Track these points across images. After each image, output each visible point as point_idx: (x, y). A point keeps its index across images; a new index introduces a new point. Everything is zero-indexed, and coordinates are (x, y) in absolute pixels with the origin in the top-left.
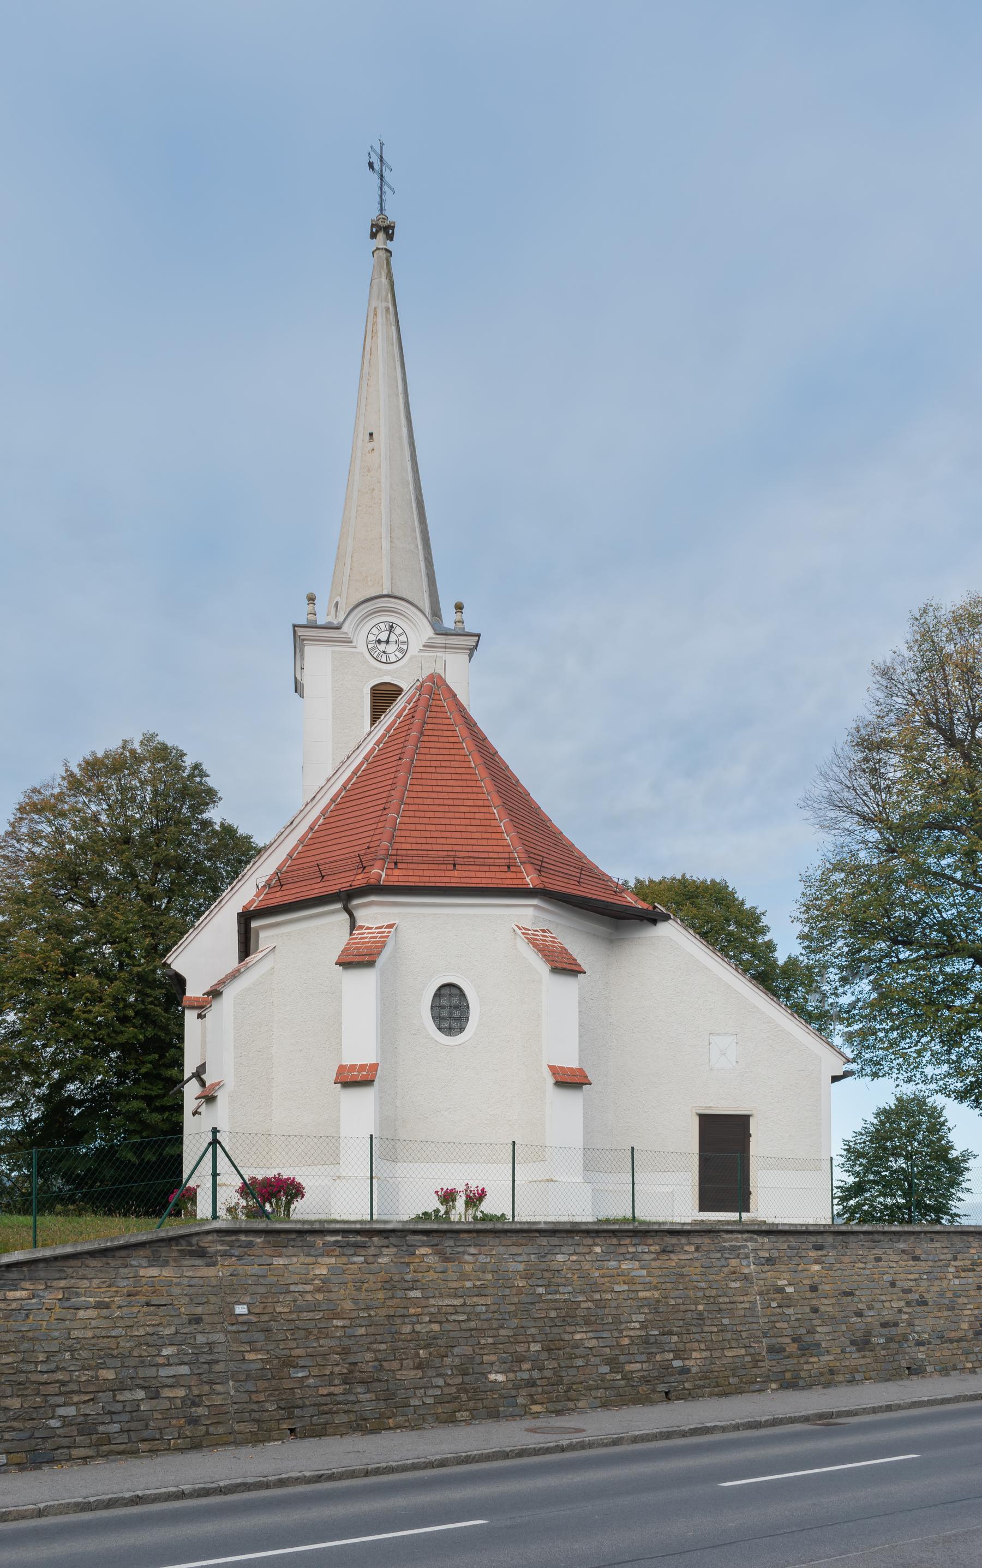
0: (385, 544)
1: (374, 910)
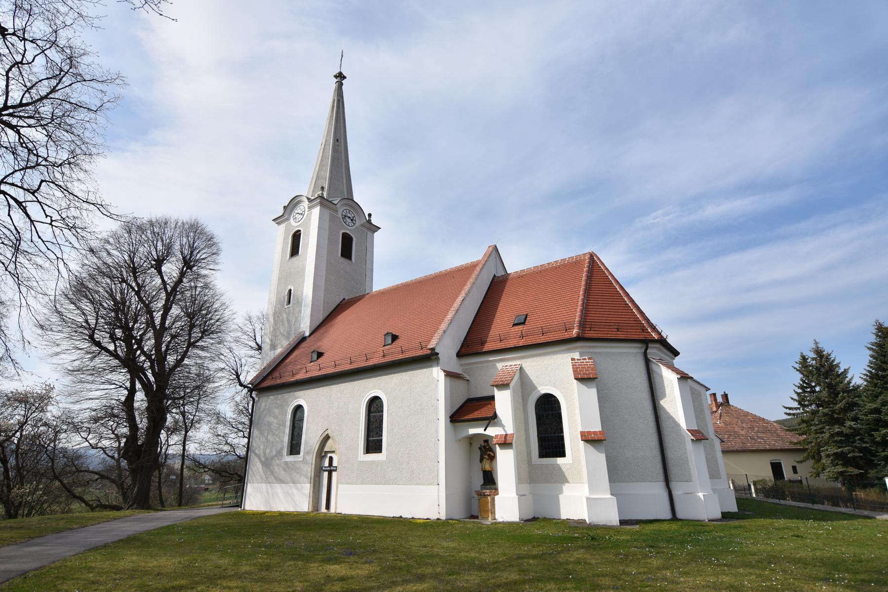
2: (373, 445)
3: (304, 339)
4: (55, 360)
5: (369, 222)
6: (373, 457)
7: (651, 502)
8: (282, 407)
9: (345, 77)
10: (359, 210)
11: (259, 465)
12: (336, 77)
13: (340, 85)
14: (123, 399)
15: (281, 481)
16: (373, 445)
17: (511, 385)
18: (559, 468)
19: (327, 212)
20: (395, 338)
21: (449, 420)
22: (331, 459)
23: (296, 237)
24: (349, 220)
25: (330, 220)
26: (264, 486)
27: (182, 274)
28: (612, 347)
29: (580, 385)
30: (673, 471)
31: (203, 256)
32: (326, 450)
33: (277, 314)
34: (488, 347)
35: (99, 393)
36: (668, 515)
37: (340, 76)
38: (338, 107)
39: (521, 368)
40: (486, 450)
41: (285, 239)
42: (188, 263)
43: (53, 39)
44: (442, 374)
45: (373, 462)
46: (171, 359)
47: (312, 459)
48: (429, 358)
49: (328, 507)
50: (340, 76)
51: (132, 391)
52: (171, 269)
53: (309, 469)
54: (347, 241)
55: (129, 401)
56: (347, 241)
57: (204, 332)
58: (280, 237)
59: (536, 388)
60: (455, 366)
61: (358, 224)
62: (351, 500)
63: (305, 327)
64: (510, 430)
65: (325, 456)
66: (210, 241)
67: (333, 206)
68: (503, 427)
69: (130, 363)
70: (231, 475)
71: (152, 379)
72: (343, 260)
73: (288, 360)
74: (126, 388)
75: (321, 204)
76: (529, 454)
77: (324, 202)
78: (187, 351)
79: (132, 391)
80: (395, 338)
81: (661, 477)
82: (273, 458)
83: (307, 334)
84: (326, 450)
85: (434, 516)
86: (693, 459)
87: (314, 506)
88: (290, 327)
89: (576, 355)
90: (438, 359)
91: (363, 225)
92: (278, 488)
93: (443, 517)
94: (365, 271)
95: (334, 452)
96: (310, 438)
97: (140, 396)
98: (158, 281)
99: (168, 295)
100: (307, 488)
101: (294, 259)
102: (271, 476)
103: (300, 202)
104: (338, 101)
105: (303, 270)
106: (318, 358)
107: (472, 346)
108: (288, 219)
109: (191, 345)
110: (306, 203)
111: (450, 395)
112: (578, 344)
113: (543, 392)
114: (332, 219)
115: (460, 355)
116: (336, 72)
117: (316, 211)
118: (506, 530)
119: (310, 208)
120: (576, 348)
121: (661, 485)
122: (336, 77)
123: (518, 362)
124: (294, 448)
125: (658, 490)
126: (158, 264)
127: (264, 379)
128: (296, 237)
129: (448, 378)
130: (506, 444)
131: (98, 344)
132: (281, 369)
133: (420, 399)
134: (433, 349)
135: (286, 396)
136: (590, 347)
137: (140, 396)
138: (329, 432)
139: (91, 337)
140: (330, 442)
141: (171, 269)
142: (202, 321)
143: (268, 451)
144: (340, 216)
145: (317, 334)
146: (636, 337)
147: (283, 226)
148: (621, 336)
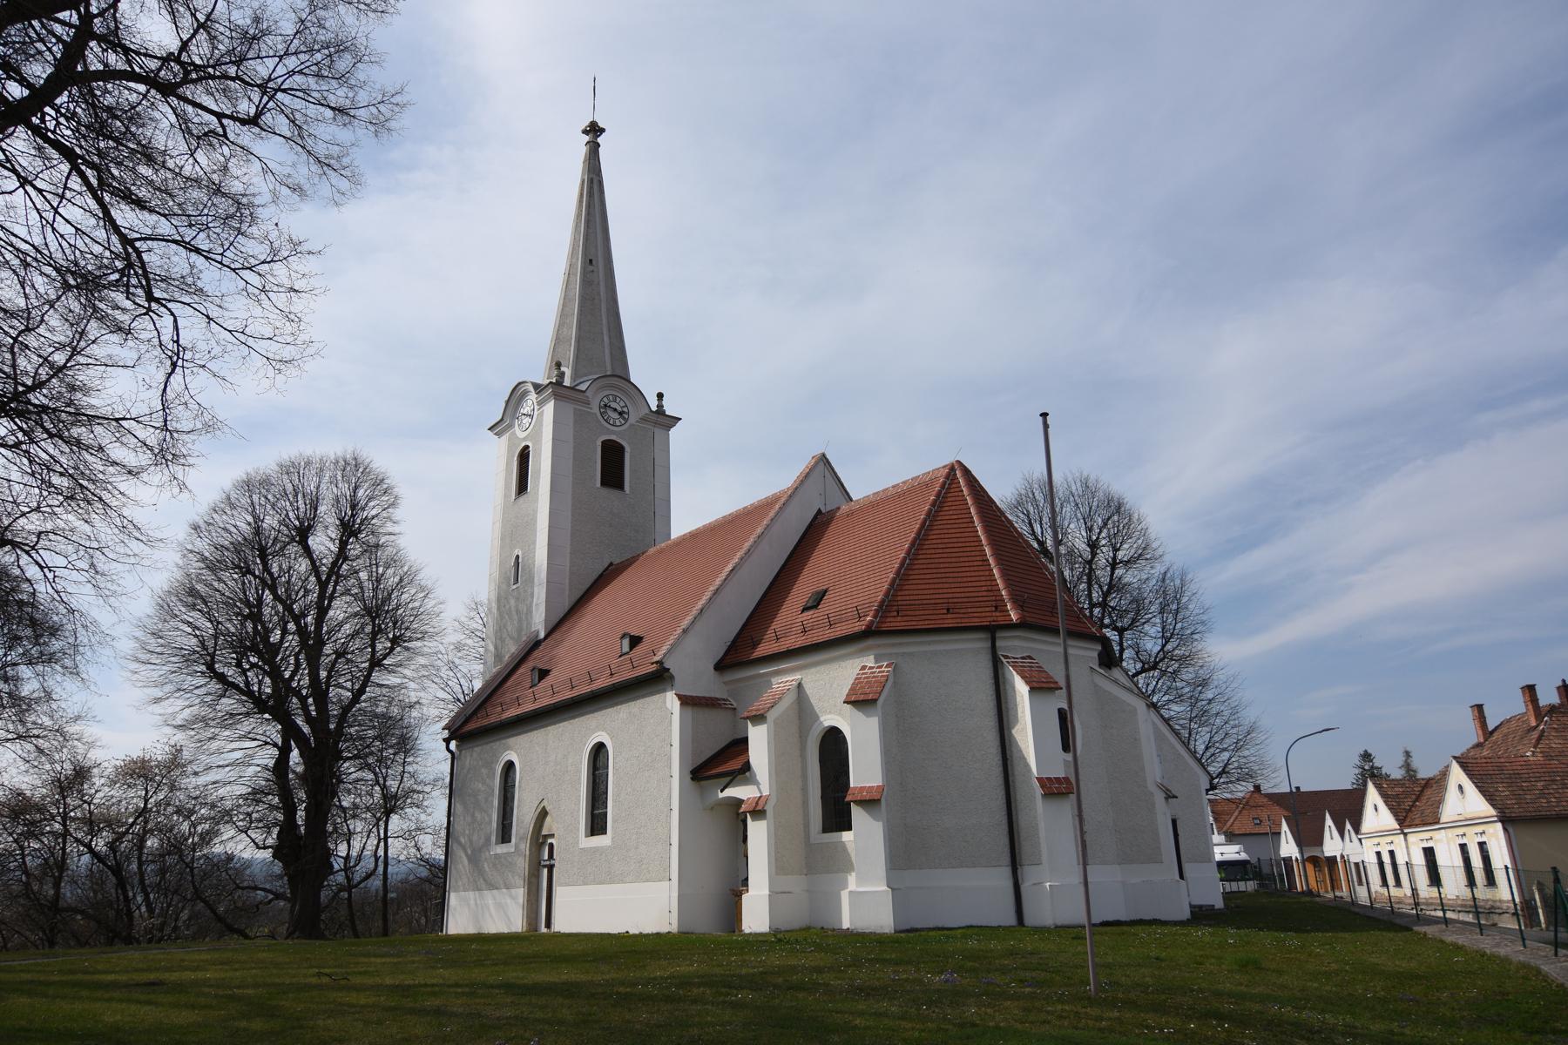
0: (606, 339)
1: (1016, 643)
2: (597, 825)
3: (537, 644)
4: (157, 708)
5: (660, 411)
6: (598, 841)
7: (973, 895)
8: (490, 765)
9: (603, 130)
10: (633, 392)
11: (466, 861)
12: (585, 132)
13: (594, 148)
14: (271, 763)
15: (492, 886)
16: (597, 825)
17: (771, 716)
18: (842, 846)
19: (569, 409)
20: (635, 641)
21: (689, 776)
22: (551, 846)
23: (524, 456)
24: (616, 415)
25: (575, 422)
26: (471, 894)
27: (343, 545)
28: (929, 643)
29: (855, 711)
30: (1025, 848)
31: (374, 512)
32: (544, 832)
33: (501, 600)
34: (763, 650)
35: (238, 754)
36: (1011, 920)
37: (594, 130)
38: (590, 194)
39: (800, 685)
40: (737, 818)
41: (508, 464)
42: (349, 529)
43: (59, 358)
44: (677, 703)
45: (595, 850)
46: (340, 693)
47: (525, 847)
48: (658, 679)
49: (548, 925)
50: (594, 130)
51: (284, 752)
52: (323, 542)
53: (522, 864)
54: (613, 457)
55: (281, 765)
56: (613, 457)
57: (395, 641)
58: (496, 457)
59: (818, 718)
60: (708, 684)
61: (633, 419)
62: (582, 910)
63: (538, 623)
64: (766, 792)
65: (543, 843)
66: (380, 484)
67: (580, 396)
68: (757, 783)
69: (274, 706)
70: (431, 887)
71: (306, 729)
72: (606, 492)
73: (509, 683)
74: (275, 745)
75: (556, 396)
76: (807, 826)
77: (557, 389)
78: (369, 675)
79: (284, 752)
80: (635, 641)
81: (1006, 859)
82: (480, 850)
83: (542, 635)
84: (544, 832)
85: (664, 930)
86: (1051, 827)
87: (529, 924)
88: (520, 620)
89: (869, 661)
90: (672, 677)
91: (644, 419)
92: (490, 897)
93: (674, 928)
94: (657, 505)
95: (552, 836)
96: (523, 816)
97: (295, 755)
98: (303, 565)
99: (323, 585)
100: (520, 893)
101: (523, 498)
102: (483, 882)
103: (525, 393)
104: (591, 181)
105: (534, 520)
106: (541, 679)
107: (740, 654)
108: (511, 426)
109: (376, 663)
110: (533, 396)
111: (691, 738)
112: (871, 642)
113: (827, 724)
114: (581, 419)
115: (721, 666)
116: (585, 123)
117: (549, 408)
118: (757, 940)
119: (541, 403)
120: (869, 648)
121: (1007, 871)
122: (585, 132)
123: (798, 676)
124: (505, 836)
125: (1000, 879)
126: (303, 534)
127: (467, 720)
128: (524, 456)
129: (689, 711)
130: (758, 813)
131: (221, 678)
132: (496, 700)
133: (651, 740)
134: (660, 663)
135: (495, 745)
136: (893, 645)
137: (295, 755)
138: (545, 803)
139: (210, 667)
140: (548, 819)
141: (323, 542)
142: (388, 625)
143: (475, 838)
144: (596, 410)
145: (557, 635)
146: (976, 622)
147: (505, 437)
148: (950, 622)
